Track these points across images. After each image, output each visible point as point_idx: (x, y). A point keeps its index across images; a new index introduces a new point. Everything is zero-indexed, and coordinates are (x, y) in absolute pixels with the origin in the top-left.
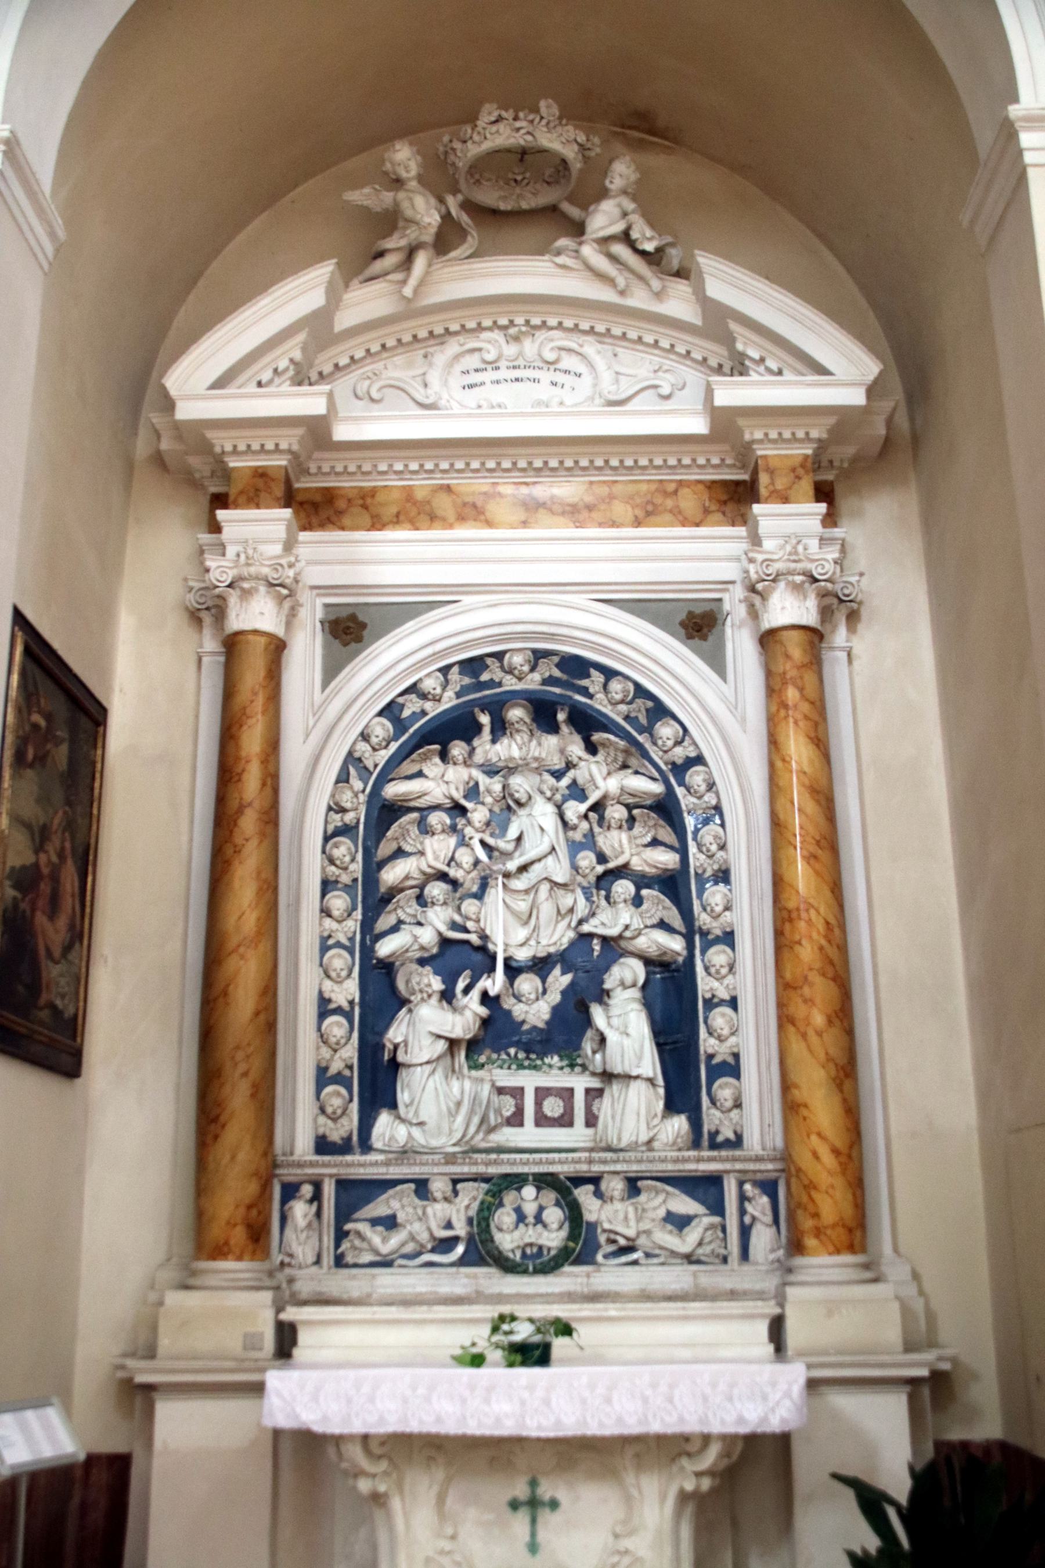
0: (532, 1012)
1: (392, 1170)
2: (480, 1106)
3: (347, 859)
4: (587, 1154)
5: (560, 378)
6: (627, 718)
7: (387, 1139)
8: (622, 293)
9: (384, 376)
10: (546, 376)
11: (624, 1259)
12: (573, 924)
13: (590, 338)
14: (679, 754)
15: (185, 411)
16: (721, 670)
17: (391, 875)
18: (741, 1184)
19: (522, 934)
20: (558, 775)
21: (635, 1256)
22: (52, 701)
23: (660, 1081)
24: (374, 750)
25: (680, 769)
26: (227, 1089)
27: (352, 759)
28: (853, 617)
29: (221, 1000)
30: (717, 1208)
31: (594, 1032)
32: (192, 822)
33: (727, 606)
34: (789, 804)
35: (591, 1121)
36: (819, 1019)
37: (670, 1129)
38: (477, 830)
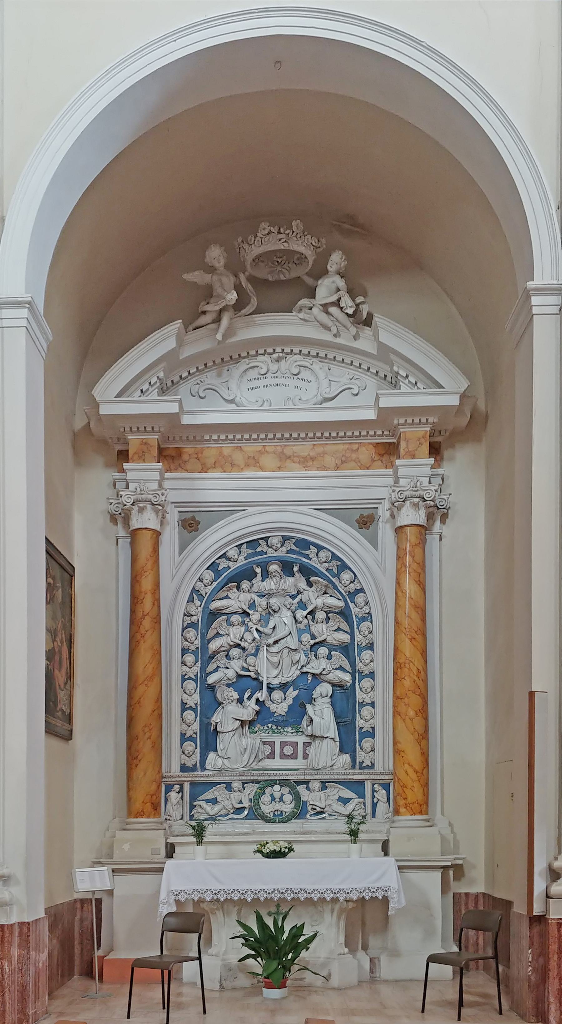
0: (279, 708)
1: (215, 778)
2: (255, 750)
3: (194, 638)
4: (303, 771)
5: (300, 383)
6: (327, 570)
7: (213, 765)
8: (335, 336)
9: (206, 383)
10: (292, 382)
11: (319, 817)
12: (299, 668)
13: (315, 360)
14: (352, 588)
15: (104, 410)
16: (375, 546)
17: (213, 646)
18: (373, 785)
19: (275, 672)
20: (293, 597)
21: (324, 815)
22: (57, 571)
23: (337, 739)
24: (205, 586)
25: (352, 595)
26: (141, 744)
27: (195, 591)
28: (444, 518)
29: (137, 705)
30: (362, 795)
31: (308, 717)
32: (117, 621)
33: (380, 512)
34: (403, 613)
35: (305, 756)
36: (411, 713)
37: (341, 760)
38: (255, 624)
